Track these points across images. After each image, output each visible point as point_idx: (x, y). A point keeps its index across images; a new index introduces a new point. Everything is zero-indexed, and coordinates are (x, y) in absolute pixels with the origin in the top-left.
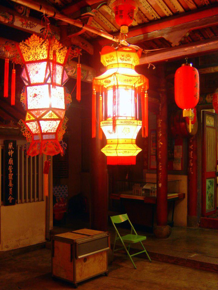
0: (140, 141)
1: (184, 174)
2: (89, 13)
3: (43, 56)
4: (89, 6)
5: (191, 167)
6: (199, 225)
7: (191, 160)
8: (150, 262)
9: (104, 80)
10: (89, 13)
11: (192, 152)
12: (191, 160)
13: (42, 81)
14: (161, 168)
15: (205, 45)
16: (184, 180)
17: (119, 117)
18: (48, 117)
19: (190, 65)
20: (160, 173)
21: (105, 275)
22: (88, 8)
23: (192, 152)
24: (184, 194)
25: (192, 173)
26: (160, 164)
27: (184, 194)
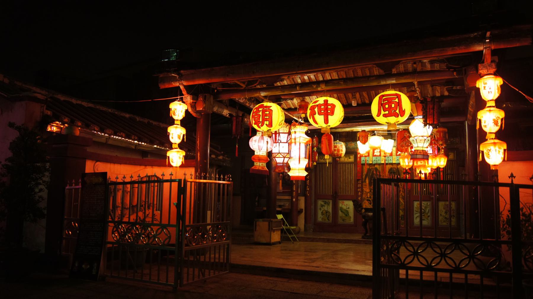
0: (307, 169)
1: (303, 196)
2: (282, 102)
3: (286, 131)
4: (282, 99)
5: (308, 191)
6: (312, 230)
7: (308, 186)
8: (298, 242)
9: (421, 154)
10: (282, 102)
11: (308, 181)
12: (308, 186)
13: (286, 142)
14: (295, 189)
15: (357, 123)
16: (302, 200)
17: (417, 155)
18: (278, 157)
19: (215, 91)
20: (294, 192)
21: (280, 243)
22: (282, 100)
23: (308, 181)
24: (302, 209)
25: (308, 195)
26: (294, 186)
27: (302, 209)
